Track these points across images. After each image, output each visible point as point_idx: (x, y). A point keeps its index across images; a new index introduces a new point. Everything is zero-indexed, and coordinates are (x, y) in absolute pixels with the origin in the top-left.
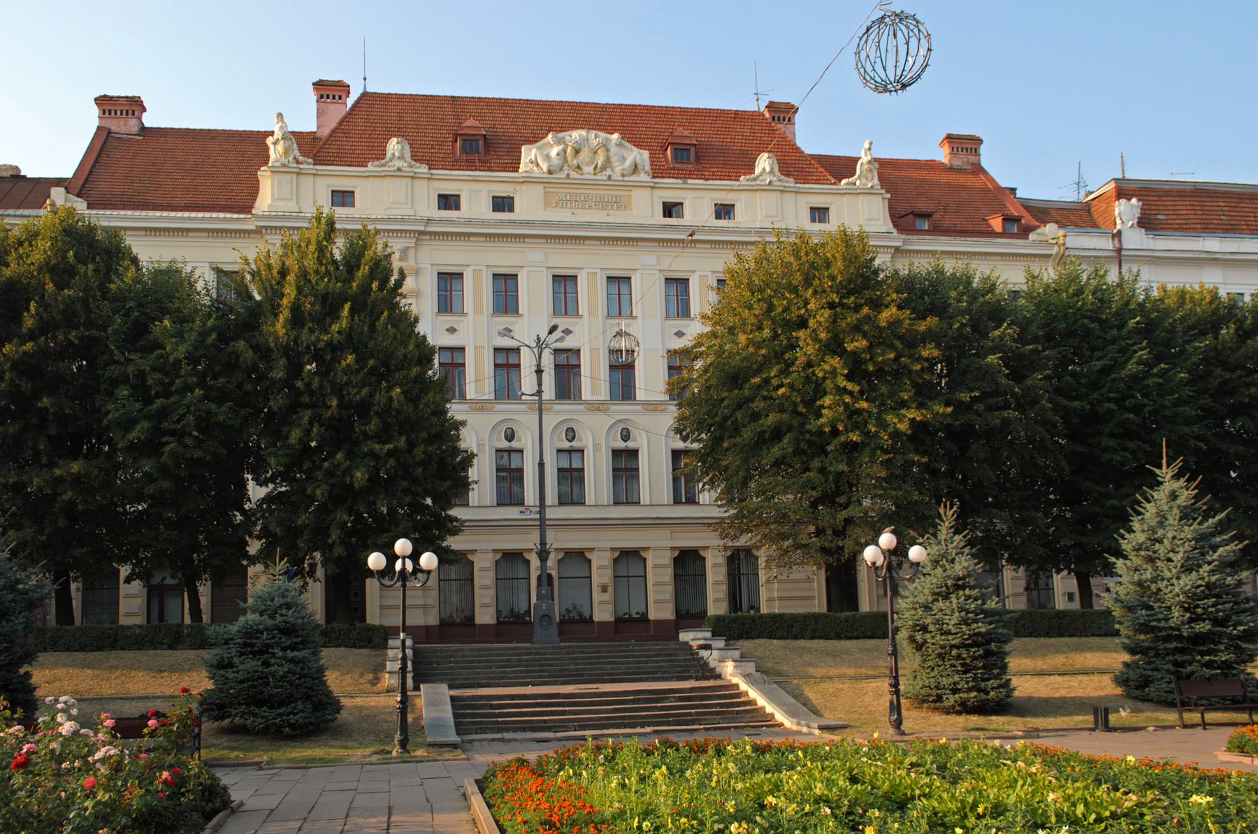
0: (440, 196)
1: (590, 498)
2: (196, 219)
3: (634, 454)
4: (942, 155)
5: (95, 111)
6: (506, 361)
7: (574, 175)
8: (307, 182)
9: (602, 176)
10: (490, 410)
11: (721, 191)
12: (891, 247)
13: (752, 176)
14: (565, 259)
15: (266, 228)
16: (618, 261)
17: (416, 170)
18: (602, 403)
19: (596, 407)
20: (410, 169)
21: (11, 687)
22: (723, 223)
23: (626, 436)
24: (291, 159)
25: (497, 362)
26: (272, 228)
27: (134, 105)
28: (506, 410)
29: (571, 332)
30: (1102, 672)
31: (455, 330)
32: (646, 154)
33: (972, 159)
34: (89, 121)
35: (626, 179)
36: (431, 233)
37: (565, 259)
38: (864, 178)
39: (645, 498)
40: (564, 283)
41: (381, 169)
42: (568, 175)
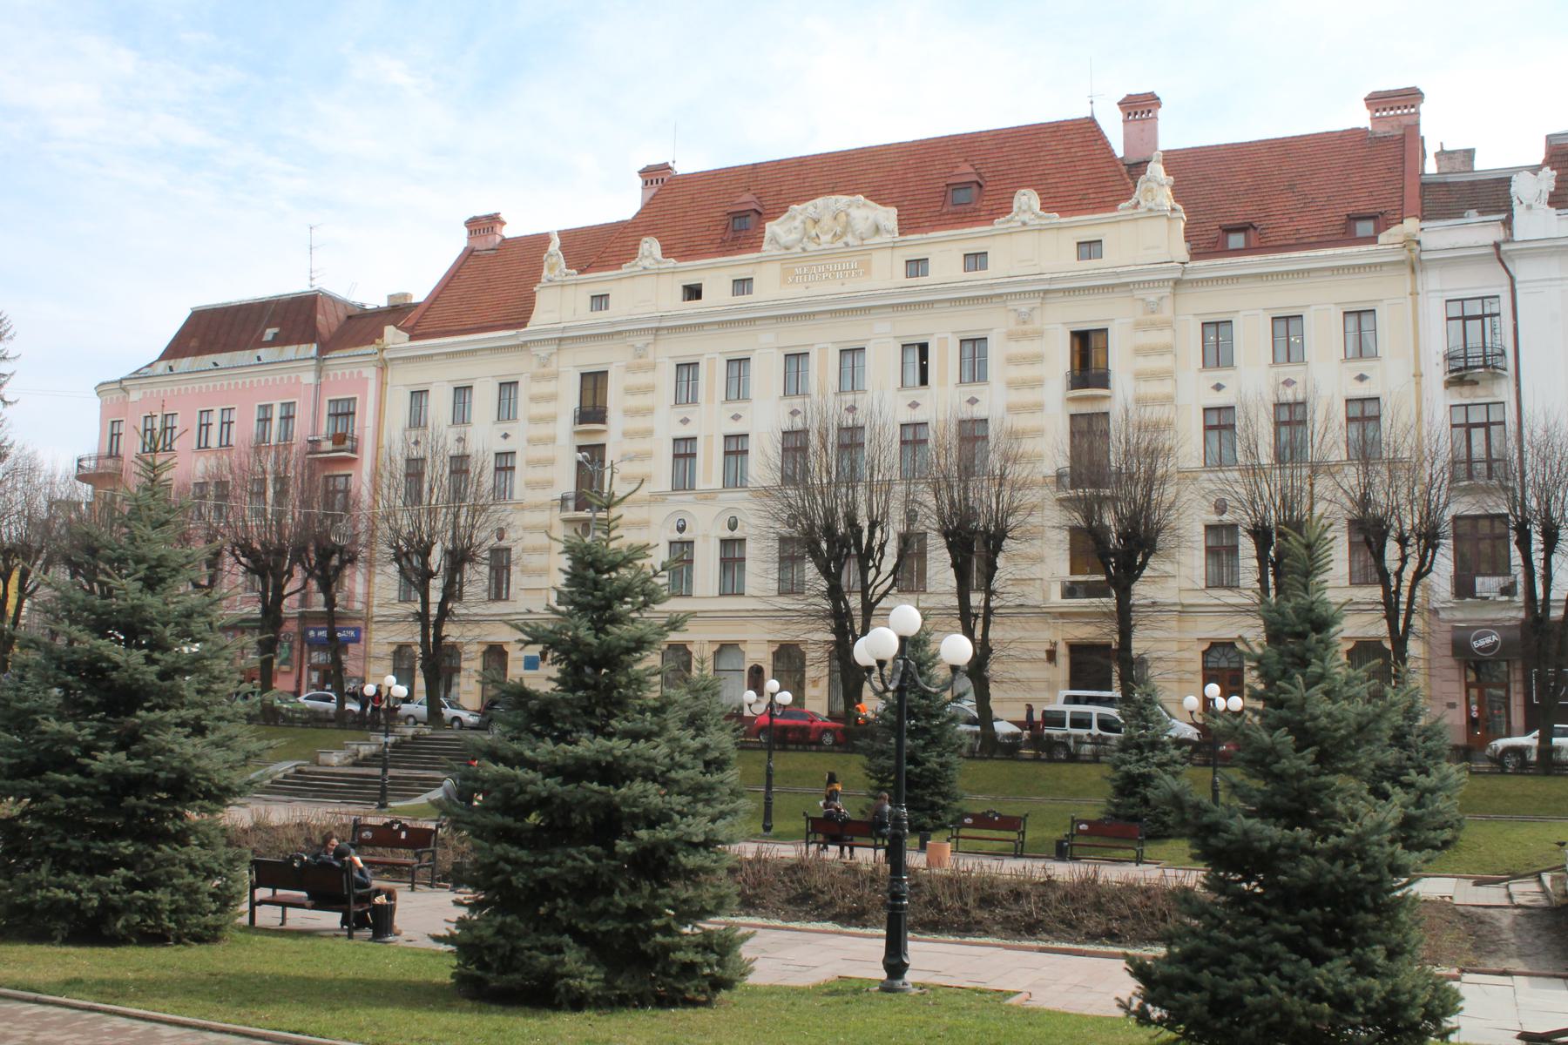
0: (685, 287)
1: (697, 589)
2: (1317, 257)
3: (690, 543)
4: (1361, 119)
5: (465, 231)
6: (736, 448)
7: (812, 247)
8: (570, 291)
9: (840, 244)
10: (714, 499)
11: (971, 237)
12: (1168, 280)
13: (1008, 217)
14: (795, 338)
15: (530, 341)
16: (850, 332)
17: (661, 266)
18: (713, 492)
19: (709, 495)
20: (1037, 222)
21: (1276, 768)
22: (972, 275)
23: (733, 526)
24: (557, 272)
25: (1208, 424)
26: (534, 341)
27: (494, 220)
28: (684, 503)
29: (977, 401)
30: (1017, 700)
31: (918, 405)
32: (893, 212)
33: (1406, 121)
34: (459, 241)
35: (865, 242)
36: (668, 328)
37: (795, 338)
38: (1157, 186)
39: (748, 590)
40: (1287, 325)
41: (1005, 226)
42: (804, 250)
